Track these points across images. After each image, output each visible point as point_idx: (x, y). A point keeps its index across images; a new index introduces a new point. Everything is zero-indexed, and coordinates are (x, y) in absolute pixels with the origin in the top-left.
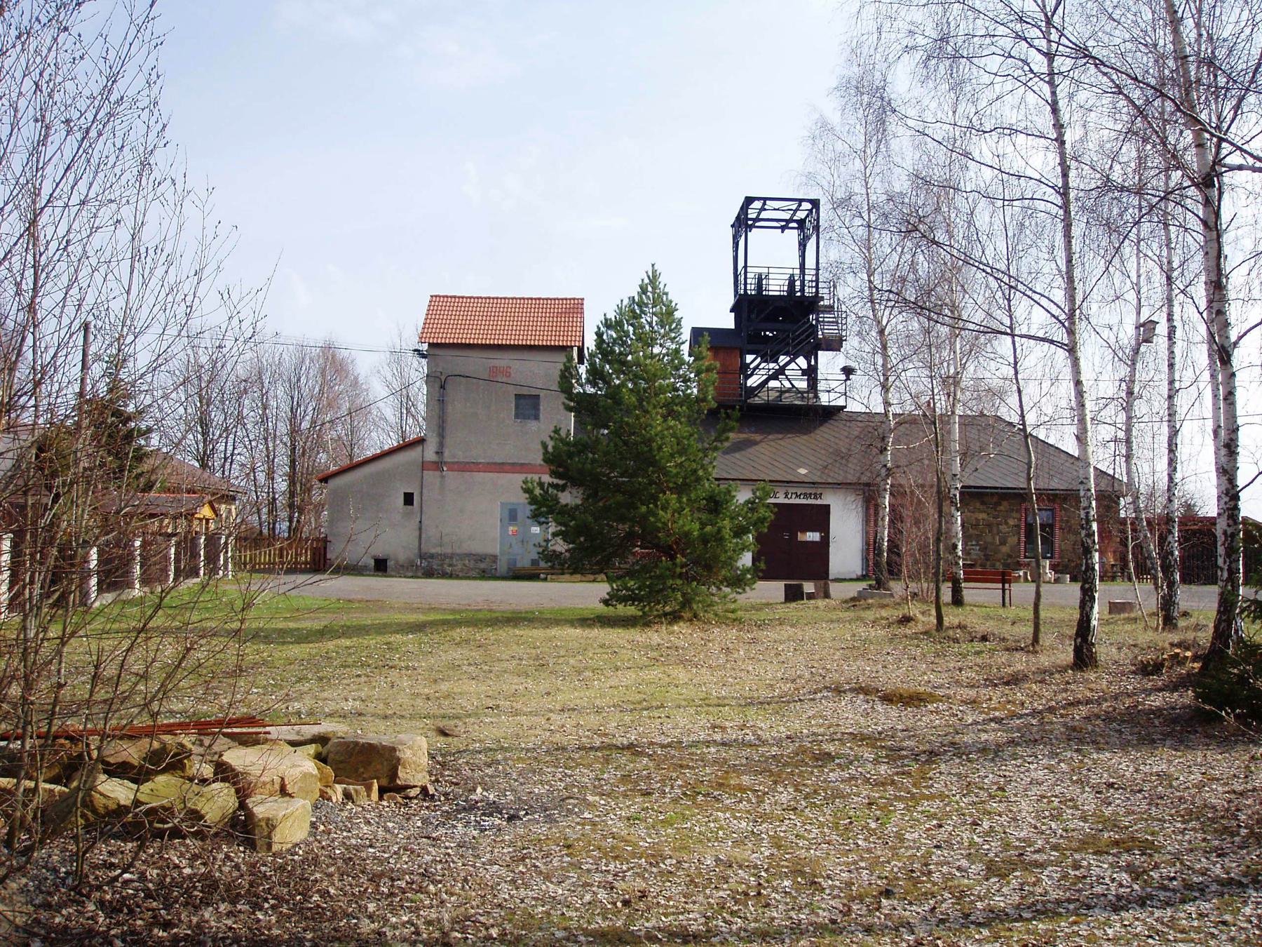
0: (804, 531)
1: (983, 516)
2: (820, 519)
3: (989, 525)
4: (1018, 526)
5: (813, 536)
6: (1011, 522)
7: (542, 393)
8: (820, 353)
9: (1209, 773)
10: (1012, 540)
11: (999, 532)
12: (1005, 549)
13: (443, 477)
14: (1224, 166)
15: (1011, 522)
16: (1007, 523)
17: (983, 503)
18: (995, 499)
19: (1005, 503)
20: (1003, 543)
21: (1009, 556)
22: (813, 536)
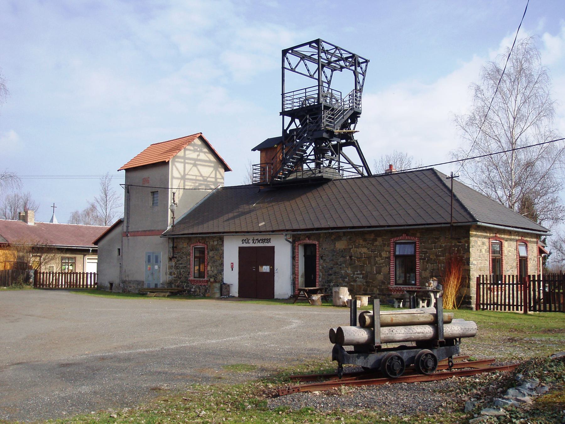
0: (262, 265)
1: (364, 250)
2: (268, 255)
3: (369, 258)
4: (389, 258)
5: (266, 269)
6: (384, 255)
7: (159, 190)
8: (280, 134)
9: (554, 319)
10: (385, 270)
11: (376, 263)
12: (380, 277)
13: (128, 240)
14: (359, 172)
15: (384, 255)
16: (381, 256)
17: (365, 240)
18: (372, 236)
19: (379, 239)
20: (379, 272)
21: (383, 283)
22: (266, 269)
